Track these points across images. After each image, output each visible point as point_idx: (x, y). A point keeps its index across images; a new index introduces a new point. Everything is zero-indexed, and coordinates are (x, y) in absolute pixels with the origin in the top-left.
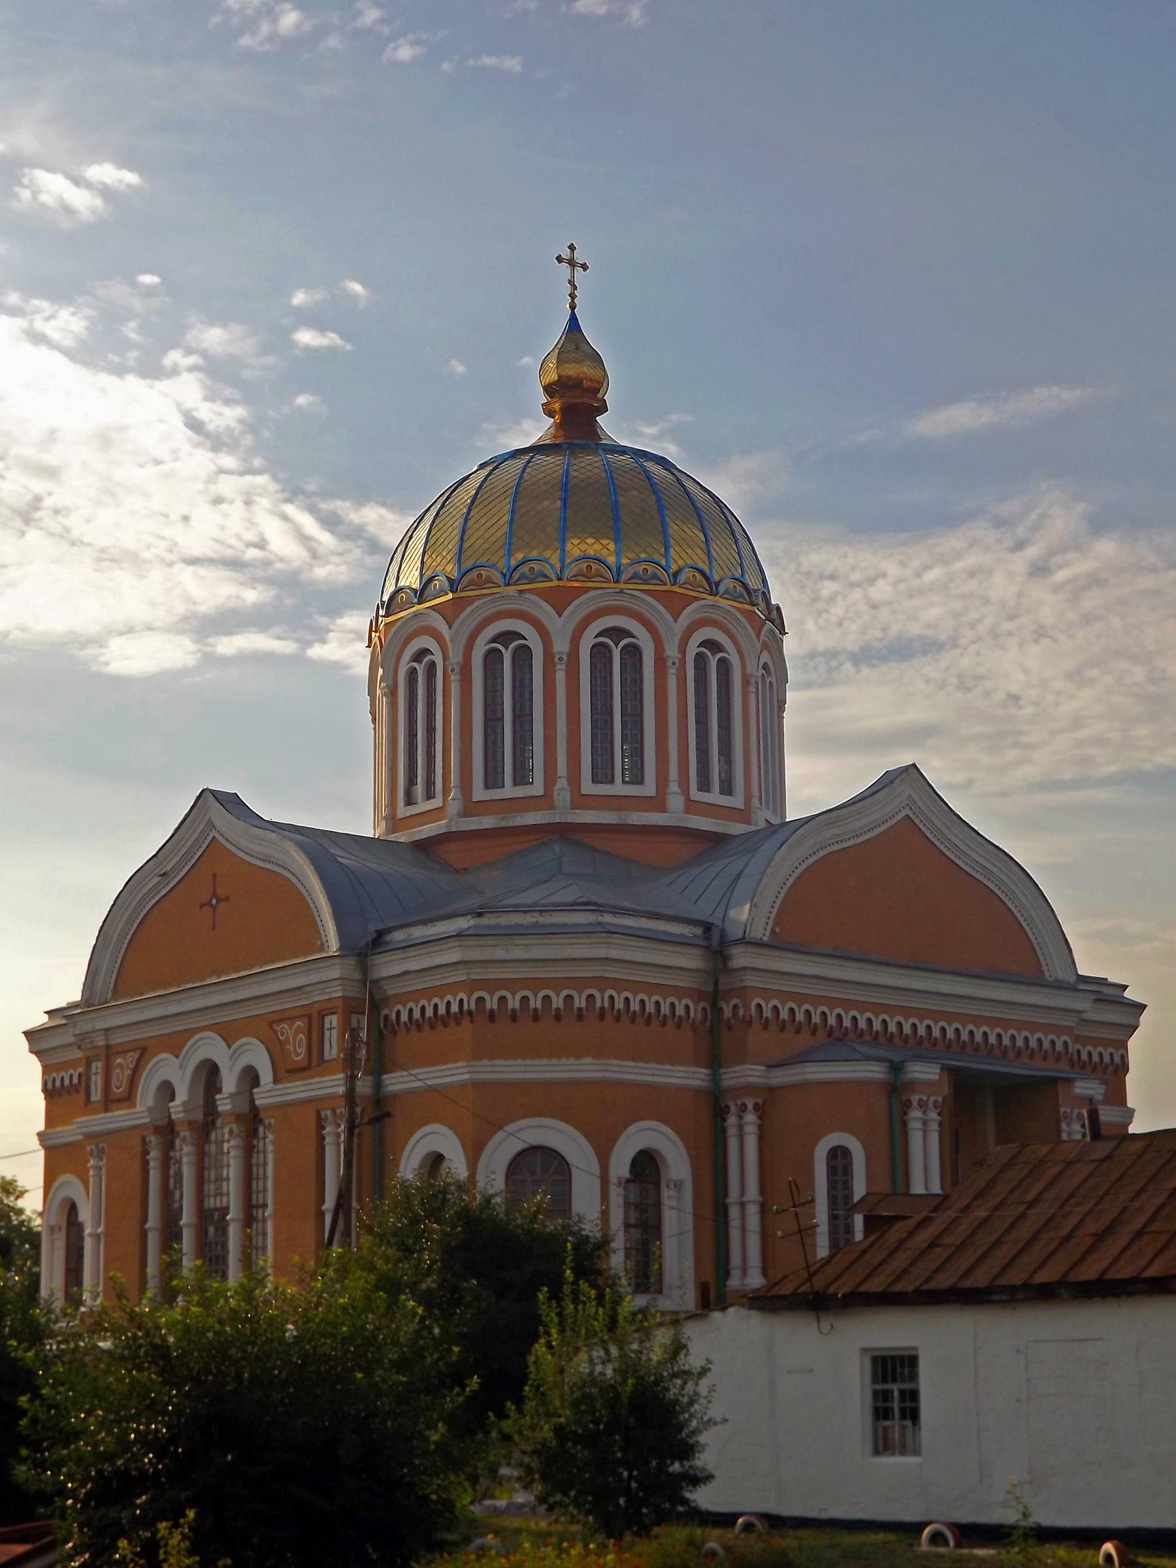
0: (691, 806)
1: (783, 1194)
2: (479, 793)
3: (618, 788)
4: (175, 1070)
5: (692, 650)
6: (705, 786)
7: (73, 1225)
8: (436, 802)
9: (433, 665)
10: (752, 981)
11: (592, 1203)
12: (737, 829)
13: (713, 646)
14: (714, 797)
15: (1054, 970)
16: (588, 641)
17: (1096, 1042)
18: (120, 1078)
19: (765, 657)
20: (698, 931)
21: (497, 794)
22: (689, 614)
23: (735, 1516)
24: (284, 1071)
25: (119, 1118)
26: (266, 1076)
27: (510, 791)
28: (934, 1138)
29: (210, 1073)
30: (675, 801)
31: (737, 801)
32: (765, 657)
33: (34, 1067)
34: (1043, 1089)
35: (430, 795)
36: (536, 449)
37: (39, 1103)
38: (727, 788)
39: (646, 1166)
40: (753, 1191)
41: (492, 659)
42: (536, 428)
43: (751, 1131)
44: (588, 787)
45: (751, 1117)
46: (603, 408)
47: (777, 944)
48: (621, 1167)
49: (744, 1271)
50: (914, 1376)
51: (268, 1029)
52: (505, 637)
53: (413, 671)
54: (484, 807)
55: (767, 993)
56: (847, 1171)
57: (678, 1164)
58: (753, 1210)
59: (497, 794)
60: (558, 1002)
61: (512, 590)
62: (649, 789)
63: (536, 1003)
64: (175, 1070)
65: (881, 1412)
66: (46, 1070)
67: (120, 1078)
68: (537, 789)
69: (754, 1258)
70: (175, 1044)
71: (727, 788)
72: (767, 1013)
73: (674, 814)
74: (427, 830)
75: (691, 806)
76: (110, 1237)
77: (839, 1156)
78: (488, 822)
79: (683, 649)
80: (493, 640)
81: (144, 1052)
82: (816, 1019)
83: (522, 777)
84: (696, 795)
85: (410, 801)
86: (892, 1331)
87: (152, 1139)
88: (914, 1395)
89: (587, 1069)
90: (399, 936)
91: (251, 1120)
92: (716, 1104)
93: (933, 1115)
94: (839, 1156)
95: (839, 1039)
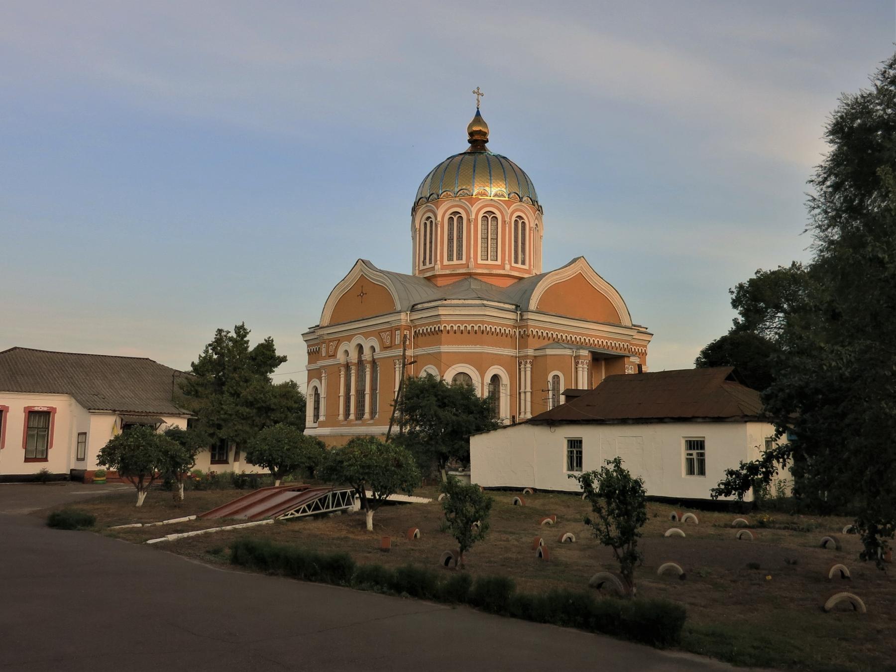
0: (512, 268)
1: (539, 389)
2: (480, 261)
3: (489, 262)
4: (351, 347)
5: (514, 219)
6: (516, 262)
7: (317, 395)
8: (432, 265)
9: (431, 222)
10: (443, 318)
11: (481, 391)
12: (526, 276)
13: (519, 217)
14: (519, 265)
15: (626, 322)
17: (637, 345)
18: (332, 349)
19: (536, 222)
20: (514, 307)
21: (451, 263)
22: (513, 207)
23: (522, 489)
24: (385, 348)
25: (330, 362)
26: (377, 349)
27: (455, 262)
28: (586, 373)
29: (360, 348)
30: (507, 267)
31: (526, 267)
32: (536, 222)
33: (305, 345)
34: (621, 358)
35: (430, 263)
36: (465, 153)
37: (306, 357)
38: (523, 263)
39: (495, 379)
40: (529, 389)
41: (451, 219)
42: (466, 147)
43: (529, 369)
44: (480, 261)
45: (529, 365)
46: (487, 141)
47: (538, 312)
48: (488, 379)
50: (581, 447)
51: (378, 334)
53: (425, 224)
54: (447, 267)
55: (535, 327)
56: (558, 383)
57: (505, 379)
58: (529, 395)
59: (451, 263)
60: (469, 328)
61: (457, 199)
62: (499, 262)
63: (455, 328)
64: (351, 347)
65: (571, 458)
66: (308, 346)
67: (332, 349)
68: (464, 261)
70: (349, 339)
71: (523, 263)
72: (535, 333)
73: (507, 270)
74: (428, 274)
75: (512, 268)
76: (328, 398)
78: (448, 272)
79: (511, 219)
81: (339, 341)
82: (550, 335)
83: (460, 257)
84: (513, 265)
85: (424, 264)
86: (574, 432)
87: (342, 369)
88: (581, 452)
89: (478, 349)
90: (419, 306)
91: (374, 363)
92: (520, 360)
93: (586, 366)
95: (557, 342)
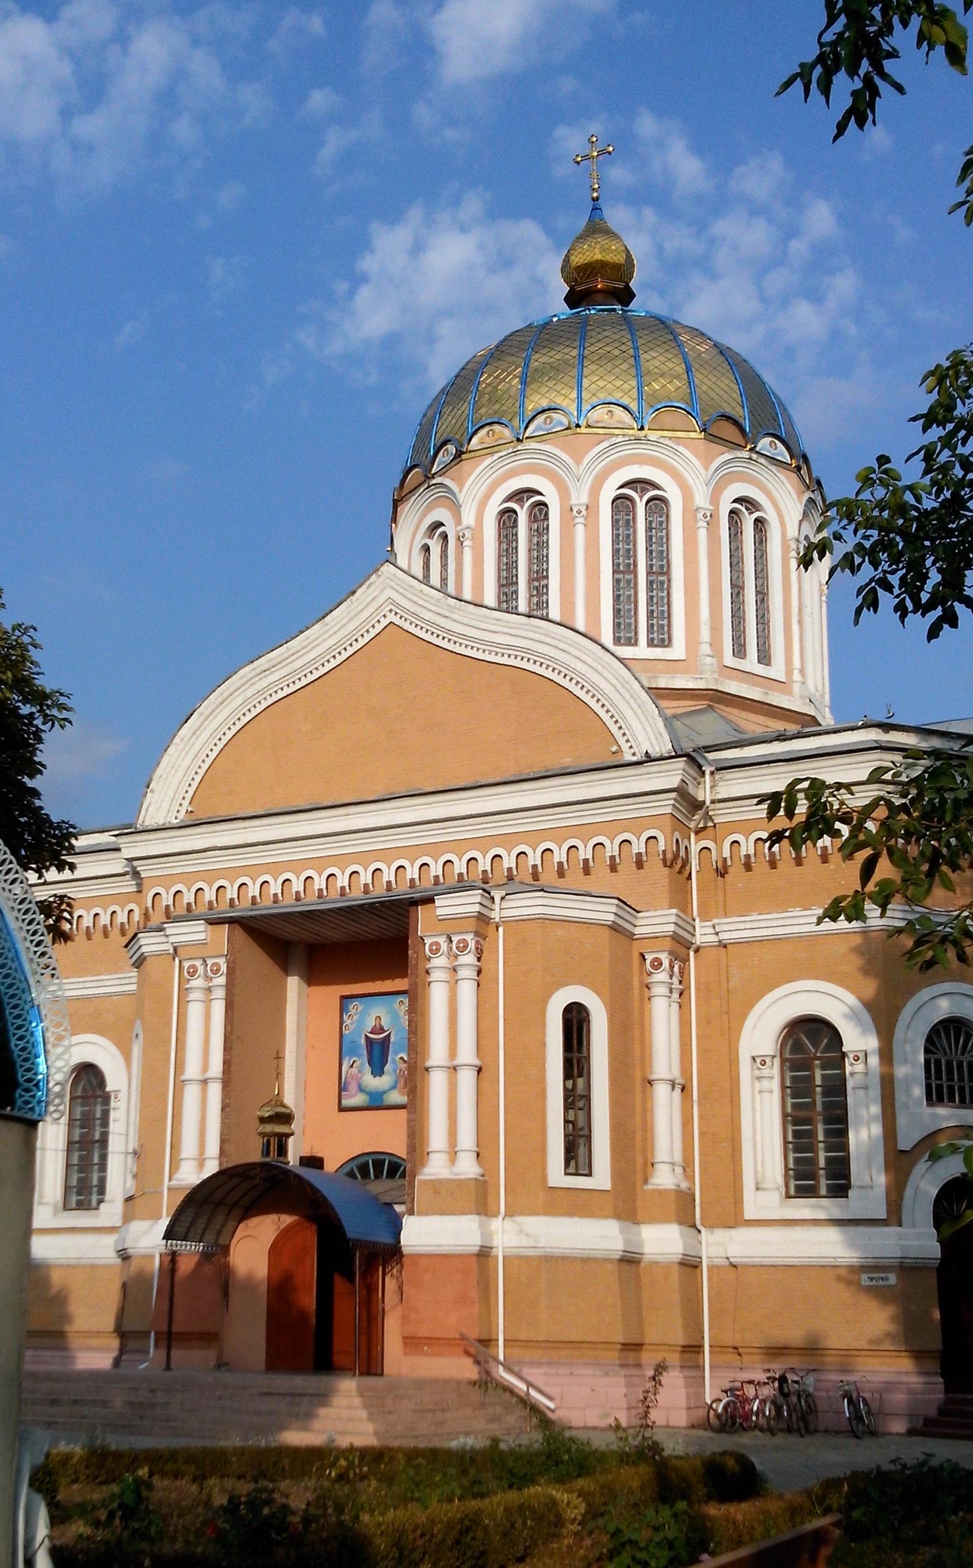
6: (740, 650)
16: (609, 491)
31: (777, 670)
49: (453, 1154)
52: (520, 495)
69: (467, 1138)
77: (576, 1020)
80: (509, 498)
94: (576, 1020)
